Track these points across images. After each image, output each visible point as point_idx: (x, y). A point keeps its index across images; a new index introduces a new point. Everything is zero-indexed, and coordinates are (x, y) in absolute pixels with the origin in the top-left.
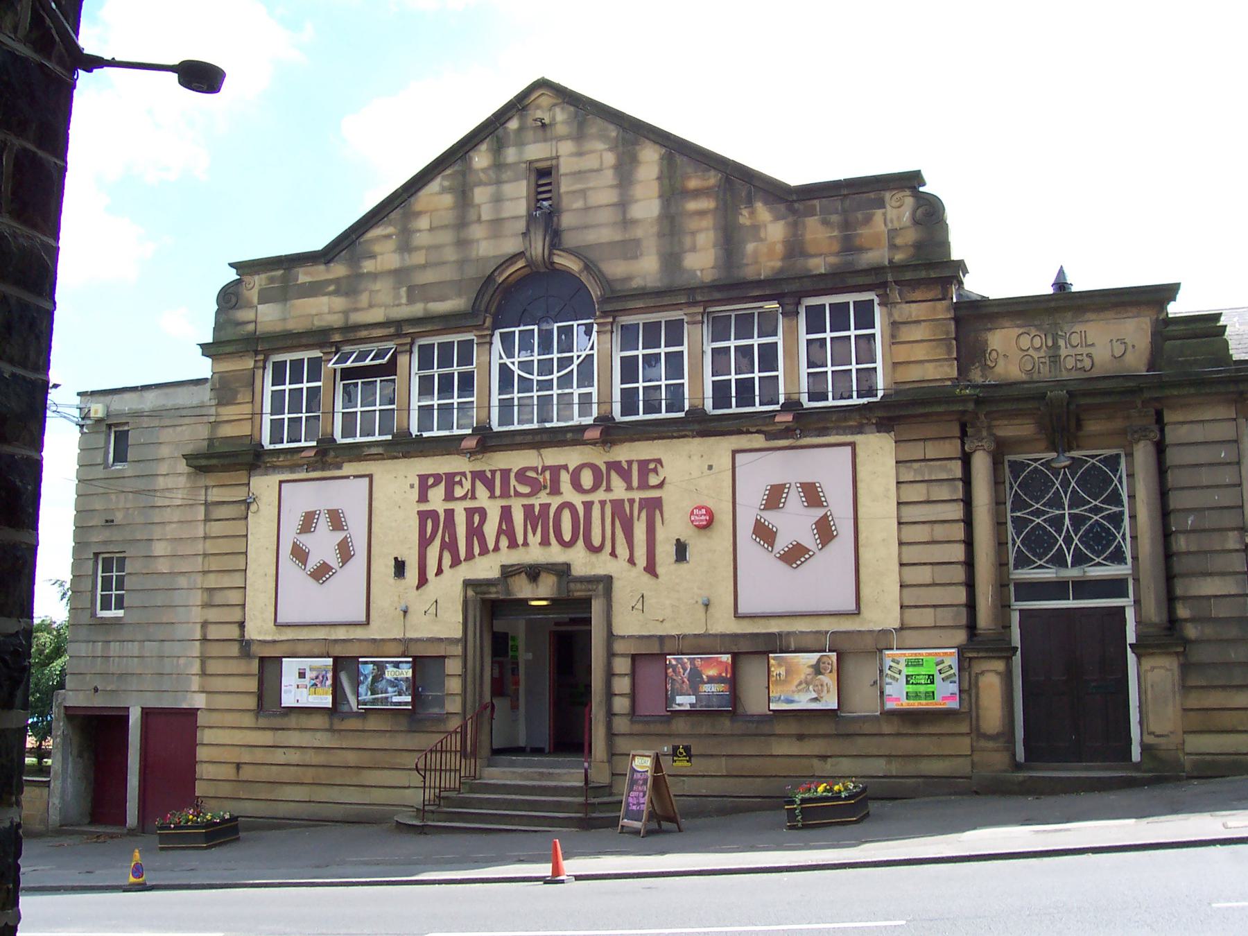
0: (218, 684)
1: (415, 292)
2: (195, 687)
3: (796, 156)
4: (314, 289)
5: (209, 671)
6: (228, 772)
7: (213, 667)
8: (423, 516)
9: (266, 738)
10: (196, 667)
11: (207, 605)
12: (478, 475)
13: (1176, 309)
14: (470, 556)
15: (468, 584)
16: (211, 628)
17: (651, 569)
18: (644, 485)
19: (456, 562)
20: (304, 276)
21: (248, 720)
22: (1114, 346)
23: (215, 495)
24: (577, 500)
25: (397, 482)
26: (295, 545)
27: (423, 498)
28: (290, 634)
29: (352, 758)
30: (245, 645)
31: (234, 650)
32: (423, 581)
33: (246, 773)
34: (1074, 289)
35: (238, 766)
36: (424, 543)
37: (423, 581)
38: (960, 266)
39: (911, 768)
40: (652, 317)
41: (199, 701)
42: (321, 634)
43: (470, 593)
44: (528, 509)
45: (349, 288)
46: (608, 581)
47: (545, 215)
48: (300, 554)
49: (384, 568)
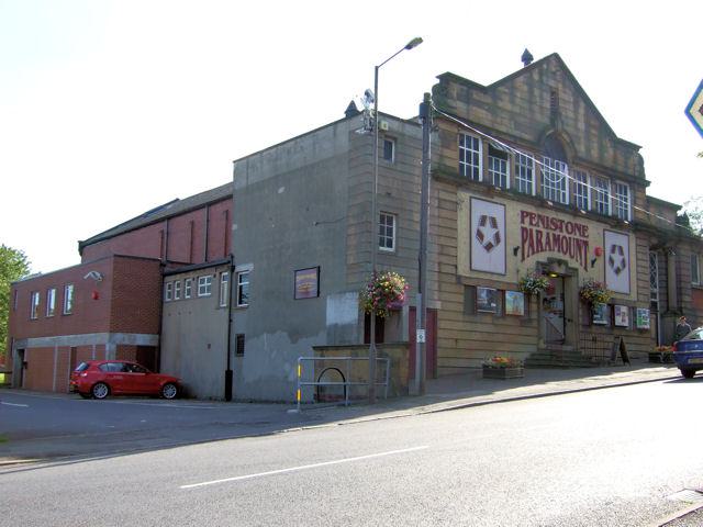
0: (445, 296)
1: (518, 126)
2: (436, 298)
3: (621, 132)
4: (480, 104)
5: (443, 289)
6: (451, 344)
7: (443, 205)
8: (524, 229)
9: (469, 327)
10: (436, 286)
11: (441, 254)
12: (539, 216)
13: (680, 213)
14: (538, 251)
15: (538, 263)
16: (442, 266)
17: (586, 268)
18: (584, 236)
19: (533, 253)
20: (476, 96)
21: (461, 317)
22: (667, 220)
23: (443, 195)
24: (567, 236)
25: (515, 209)
26: (478, 231)
27: (523, 222)
28: (475, 275)
29: (500, 337)
30: (459, 278)
31: (454, 280)
32: (523, 259)
33: (461, 344)
34: (650, 192)
35: (456, 340)
36: (524, 242)
37: (523, 259)
38: (648, 183)
39: (639, 348)
40: (629, 200)
41: (438, 305)
42: (488, 277)
43: (540, 267)
44: (554, 235)
45: (493, 110)
46: (577, 270)
47: (555, 113)
48: (480, 236)
49: (510, 251)
